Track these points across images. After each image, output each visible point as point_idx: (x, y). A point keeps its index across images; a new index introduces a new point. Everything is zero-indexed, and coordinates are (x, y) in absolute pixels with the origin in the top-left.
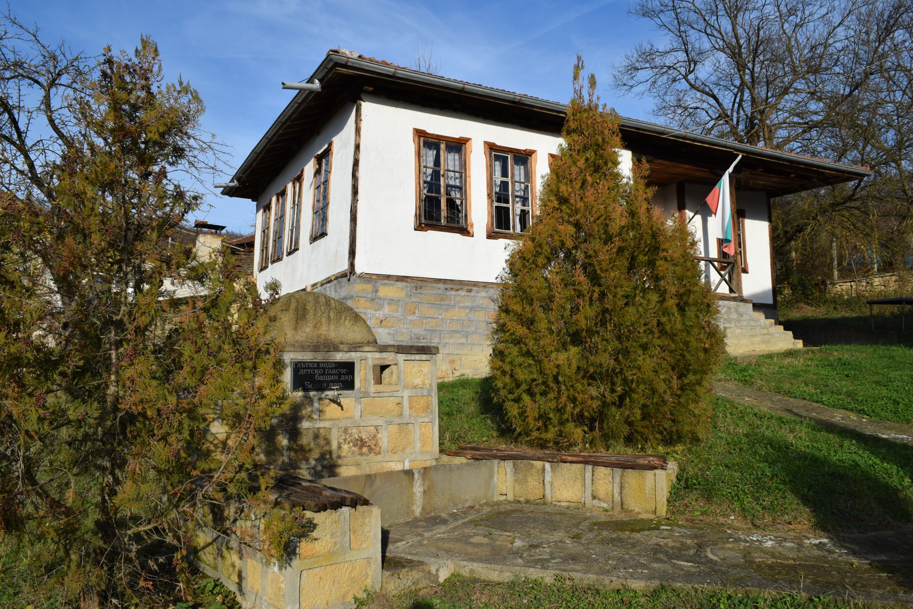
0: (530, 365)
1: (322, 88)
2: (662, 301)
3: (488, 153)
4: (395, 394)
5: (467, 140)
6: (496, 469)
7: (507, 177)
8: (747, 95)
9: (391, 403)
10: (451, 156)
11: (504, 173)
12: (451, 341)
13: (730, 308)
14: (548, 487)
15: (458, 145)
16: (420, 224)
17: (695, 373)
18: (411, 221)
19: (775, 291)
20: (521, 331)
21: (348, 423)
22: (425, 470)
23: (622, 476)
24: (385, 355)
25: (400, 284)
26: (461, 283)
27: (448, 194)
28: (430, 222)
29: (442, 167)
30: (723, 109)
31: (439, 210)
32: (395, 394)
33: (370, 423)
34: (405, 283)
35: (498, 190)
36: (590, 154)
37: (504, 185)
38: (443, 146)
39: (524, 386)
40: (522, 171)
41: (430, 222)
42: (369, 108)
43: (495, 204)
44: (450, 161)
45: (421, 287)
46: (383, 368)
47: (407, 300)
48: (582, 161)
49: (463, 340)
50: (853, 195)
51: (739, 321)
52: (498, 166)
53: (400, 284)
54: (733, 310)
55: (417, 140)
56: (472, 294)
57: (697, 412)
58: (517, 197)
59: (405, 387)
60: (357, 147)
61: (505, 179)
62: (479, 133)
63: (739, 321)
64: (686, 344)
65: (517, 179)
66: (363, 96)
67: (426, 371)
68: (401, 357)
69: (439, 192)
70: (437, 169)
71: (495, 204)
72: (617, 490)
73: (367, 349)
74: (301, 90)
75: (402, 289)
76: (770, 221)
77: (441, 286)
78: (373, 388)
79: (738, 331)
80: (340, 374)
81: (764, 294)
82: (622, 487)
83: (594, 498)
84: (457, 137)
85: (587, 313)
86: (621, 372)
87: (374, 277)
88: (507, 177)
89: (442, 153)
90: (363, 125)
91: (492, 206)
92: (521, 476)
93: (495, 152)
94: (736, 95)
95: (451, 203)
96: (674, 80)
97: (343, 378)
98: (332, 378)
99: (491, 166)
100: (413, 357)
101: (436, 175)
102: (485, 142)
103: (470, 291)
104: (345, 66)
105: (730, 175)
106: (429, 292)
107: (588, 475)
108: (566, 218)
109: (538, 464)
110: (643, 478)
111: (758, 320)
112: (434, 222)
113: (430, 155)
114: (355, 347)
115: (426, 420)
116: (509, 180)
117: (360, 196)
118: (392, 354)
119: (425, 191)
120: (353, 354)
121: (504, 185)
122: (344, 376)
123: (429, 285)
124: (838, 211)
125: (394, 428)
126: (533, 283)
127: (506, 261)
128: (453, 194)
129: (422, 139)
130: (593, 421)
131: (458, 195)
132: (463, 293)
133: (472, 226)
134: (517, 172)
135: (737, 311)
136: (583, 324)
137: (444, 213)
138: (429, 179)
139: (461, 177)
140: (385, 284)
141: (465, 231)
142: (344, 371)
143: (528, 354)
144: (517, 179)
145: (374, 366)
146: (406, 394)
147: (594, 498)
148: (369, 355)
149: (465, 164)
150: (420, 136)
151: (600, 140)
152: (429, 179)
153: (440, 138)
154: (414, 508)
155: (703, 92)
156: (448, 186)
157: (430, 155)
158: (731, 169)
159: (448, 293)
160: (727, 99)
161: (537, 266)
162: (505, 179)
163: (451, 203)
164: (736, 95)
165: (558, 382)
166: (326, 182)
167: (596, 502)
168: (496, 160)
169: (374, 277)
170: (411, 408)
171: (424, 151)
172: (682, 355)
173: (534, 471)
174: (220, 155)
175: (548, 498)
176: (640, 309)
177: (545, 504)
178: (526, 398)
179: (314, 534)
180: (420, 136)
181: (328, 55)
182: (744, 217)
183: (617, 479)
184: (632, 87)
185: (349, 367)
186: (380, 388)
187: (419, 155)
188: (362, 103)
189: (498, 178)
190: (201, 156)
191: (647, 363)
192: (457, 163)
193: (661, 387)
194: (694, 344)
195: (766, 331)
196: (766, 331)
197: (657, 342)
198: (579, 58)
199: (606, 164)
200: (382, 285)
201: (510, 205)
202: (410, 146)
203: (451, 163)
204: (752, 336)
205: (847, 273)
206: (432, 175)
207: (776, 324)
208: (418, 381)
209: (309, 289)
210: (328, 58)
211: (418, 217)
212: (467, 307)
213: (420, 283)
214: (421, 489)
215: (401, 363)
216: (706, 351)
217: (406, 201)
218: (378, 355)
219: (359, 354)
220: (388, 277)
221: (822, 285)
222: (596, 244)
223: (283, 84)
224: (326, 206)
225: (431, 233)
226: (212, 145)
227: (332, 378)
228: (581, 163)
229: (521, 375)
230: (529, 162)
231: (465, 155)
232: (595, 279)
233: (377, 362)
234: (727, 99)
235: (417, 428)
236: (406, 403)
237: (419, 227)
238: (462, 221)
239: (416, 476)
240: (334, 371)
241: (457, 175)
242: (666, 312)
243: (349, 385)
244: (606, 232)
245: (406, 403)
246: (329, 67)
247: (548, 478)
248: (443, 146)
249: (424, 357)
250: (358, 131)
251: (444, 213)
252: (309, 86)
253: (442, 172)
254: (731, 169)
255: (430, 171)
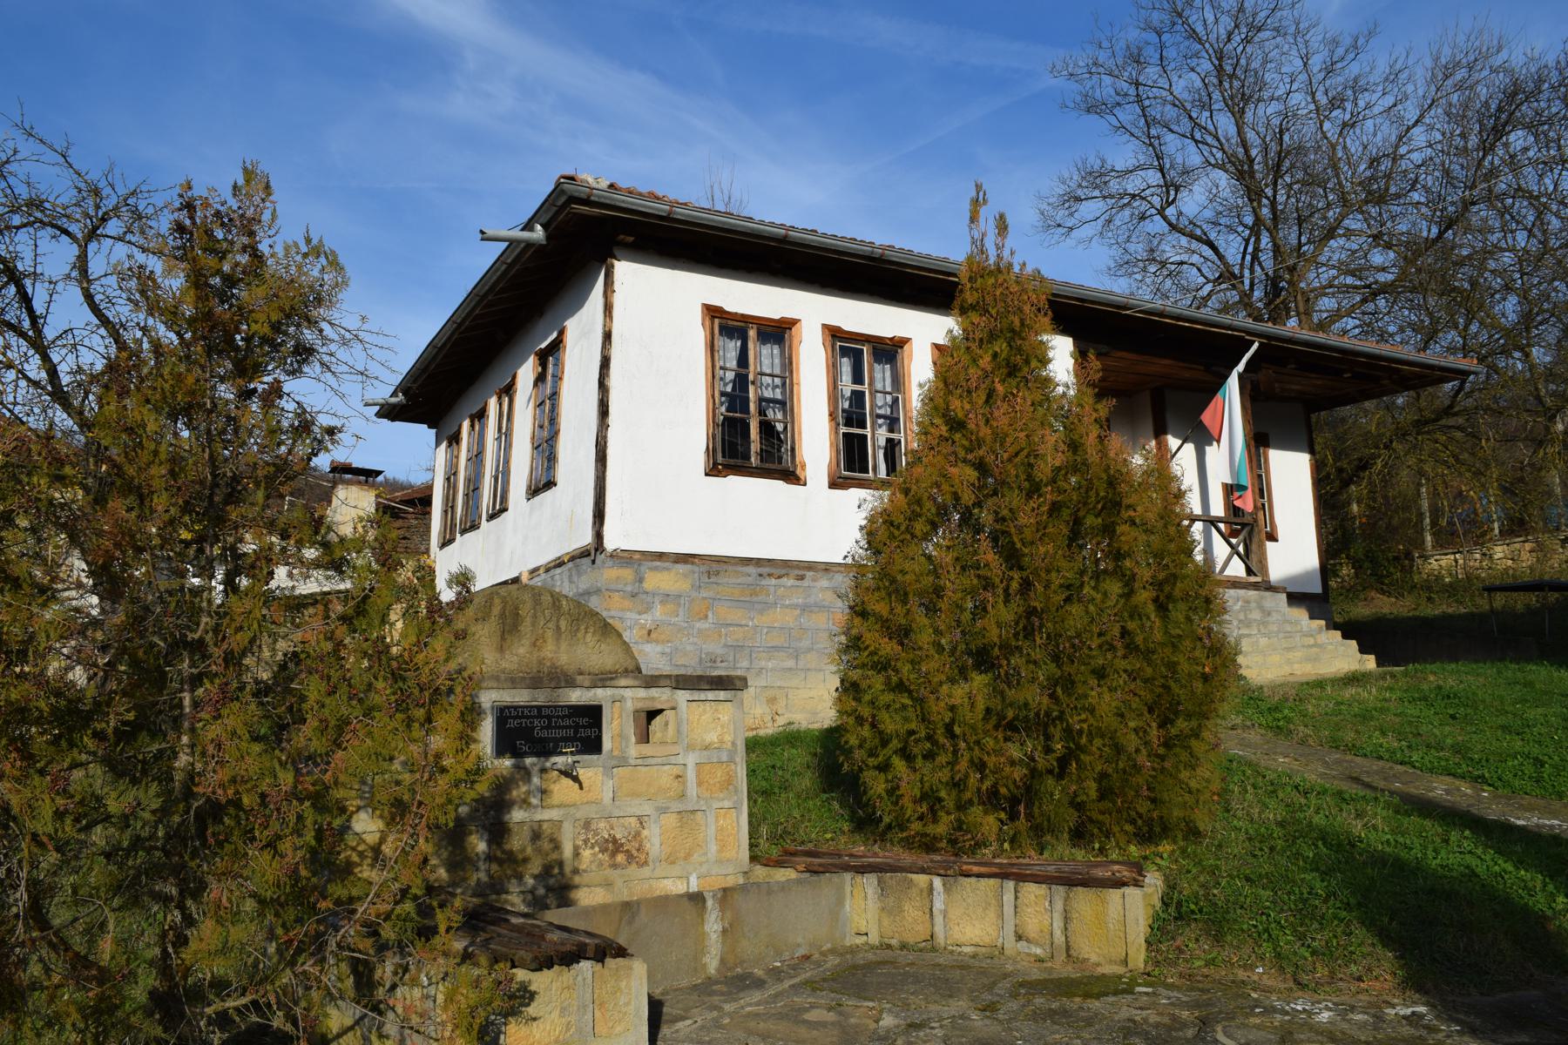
0: (904, 707)
1: (548, 238)
2: (1128, 595)
3: (828, 344)
4: (673, 760)
5: (794, 322)
6: (848, 889)
7: (862, 383)
8: (1265, 240)
9: (665, 776)
10: (766, 350)
11: (858, 378)
12: (770, 665)
13: (1248, 602)
14: (939, 919)
15: (778, 332)
16: (715, 464)
17: (1189, 716)
18: (699, 460)
19: (1326, 571)
20: (888, 647)
21: (591, 812)
22: (726, 894)
23: (1067, 899)
24: (654, 692)
25: (681, 568)
26: (786, 564)
27: (762, 412)
28: (732, 462)
29: (752, 368)
30: (1225, 263)
31: (746, 440)
32: (673, 760)
33: (630, 811)
34: (689, 567)
35: (846, 405)
36: (1000, 346)
37: (858, 397)
38: (752, 333)
39: (895, 744)
40: (888, 374)
41: (732, 462)
42: (625, 270)
43: (843, 430)
44: (765, 358)
45: (717, 573)
46: (652, 715)
47: (695, 594)
48: (988, 358)
49: (791, 663)
50: (1451, 406)
51: (1265, 624)
52: (846, 366)
53: (681, 568)
54: (1253, 605)
55: (708, 323)
56: (806, 583)
57: (1193, 784)
58: (879, 416)
59: (690, 747)
60: (607, 336)
61: (858, 387)
62: (814, 311)
63: (1265, 624)
64: (1172, 667)
65: (879, 386)
66: (616, 252)
67: (725, 718)
68: (682, 696)
69: (748, 412)
70: (743, 371)
71: (843, 430)
72: (1058, 924)
73: (623, 682)
74: (512, 242)
75: (685, 576)
76: (1312, 452)
77: (751, 570)
78: (634, 750)
79: (1263, 641)
80: (577, 727)
81: (1306, 576)
82: (1067, 919)
83: (1019, 938)
84: (777, 317)
85: (1001, 617)
86: (1061, 718)
87: (637, 556)
88: (862, 383)
89: (751, 345)
90: (618, 300)
91: (837, 433)
92: (891, 901)
93: (841, 342)
94: (1247, 241)
95: (767, 428)
96: (1143, 217)
97: (583, 733)
98: (563, 733)
99: (834, 365)
100: (702, 695)
101: (741, 381)
102: (825, 326)
103: (802, 578)
104: (586, 202)
105: (1240, 376)
106: (731, 581)
107: (1008, 897)
108: (962, 454)
109: (921, 879)
110: (1104, 902)
111: (1297, 622)
112: (739, 462)
113: (732, 348)
114: (603, 679)
115: (727, 804)
116: (865, 388)
117: (612, 419)
118: (667, 691)
119: (723, 409)
120: (599, 691)
121: (858, 397)
122: (584, 728)
123: (730, 568)
124: (1428, 433)
125: (670, 820)
126: (907, 566)
127: (862, 528)
128: (770, 413)
129: (717, 321)
130: (1015, 803)
131: (779, 416)
132: (789, 582)
133: (803, 466)
134: (878, 376)
135: (1261, 608)
136: (994, 634)
137: (755, 447)
138: (729, 389)
139: (784, 384)
140: (656, 569)
141: (791, 476)
142: (583, 721)
143: (901, 687)
144: (879, 386)
145: (636, 712)
146: (691, 760)
147: (1019, 938)
148: (628, 693)
149: (791, 363)
150: (713, 317)
151: (1017, 323)
152: (729, 389)
153: (747, 319)
154: (707, 959)
155: (1192, 236)
156: (761, 400)
157: (732, 348)
158: (1241, 367)
159: (764, 582)
160: (1232, 248)
161: (913, 536)
162: (858, 387)
163: (767, 428)
164: (1247, 241)
165: (953, 736)
166: (555, 395)
167: (1022, 945)
168: (843, 355)
169: (637, 556)
170: (700, 784)
171: (720, 341)
172: (1166, 687)
173: (914, 891)
174: (374, 351)
175: (940, 939)
176: (1091, 608)
177: (934, 949)
178: (899, 764)
179: (532, 1010)
180: (713, 317)
181: (558, 184)
182: (1267, 445)
183: (1059, 905)
184: (1071, 229)
185: (593, 714)
186: (646, 749)
187: (711, 348)
188: (616, 263)
189: (847, 386)
190: (342, 354)
191: (1104, 700)
192: (777, 361)
193: (1131, 742)
194: (1185, 667)
195: (1311, 641)
196: (1311, 641)
197: (1121, 664)
198: (978, 187)
199: (1027, 362)
200: (651, 569)
201: (868, 432)
202: (696, 335)
203: (766, 362)
204: (1288, 649)
205: (1447, 539)
206: (734, 382)
207: (1328, 628)
208: (712, 737)
209: (525, 579)
210: (558, 190)
211: (711, 452)
212: (796, 606)
213: (715, 566)
214: (718, 927)
215: (683, 705)
216: (1206, 678)
217: (690, 426)
218: (642, 693)
219: (609, 691)
220: (661, 556)
221: (1405, 561)
222: (1014, 498)
223: (482, 232)
224: (554, 435)
225: (733, 480)
226: (362, 335)
227: (563, 733)
228: (986, 361)
229: (890, 724)
230: (899, 357)
231: (790, 347)
232: (1012, 557)
233: (640, 705)
234: (1232, 248)
235: (711, 819)
236: (691, 774)
237: (713, 470)
238: (787, 458)
239: (710, 903)
240: (568, 722)
241: (777, 381)
242: (1135, 613)
243: (593, 745)
244: (1029, 478)
245: (691, 774)
246: (560, 203)
247: (938, 905)
248: (752, 333)
249: (722, 695)
250: (608, 309)
251: (755, 447)
252: (526, 235)
253: (751, 377)
254: (1241, 367)
255: (730, 376)
